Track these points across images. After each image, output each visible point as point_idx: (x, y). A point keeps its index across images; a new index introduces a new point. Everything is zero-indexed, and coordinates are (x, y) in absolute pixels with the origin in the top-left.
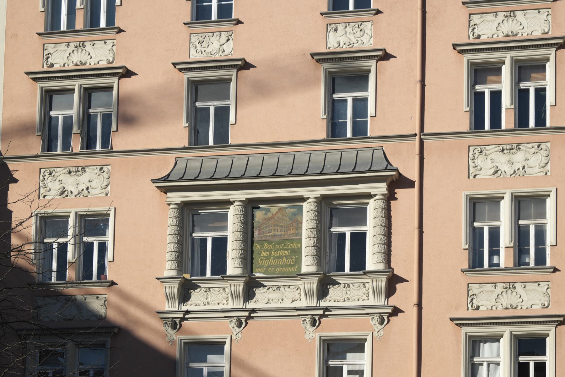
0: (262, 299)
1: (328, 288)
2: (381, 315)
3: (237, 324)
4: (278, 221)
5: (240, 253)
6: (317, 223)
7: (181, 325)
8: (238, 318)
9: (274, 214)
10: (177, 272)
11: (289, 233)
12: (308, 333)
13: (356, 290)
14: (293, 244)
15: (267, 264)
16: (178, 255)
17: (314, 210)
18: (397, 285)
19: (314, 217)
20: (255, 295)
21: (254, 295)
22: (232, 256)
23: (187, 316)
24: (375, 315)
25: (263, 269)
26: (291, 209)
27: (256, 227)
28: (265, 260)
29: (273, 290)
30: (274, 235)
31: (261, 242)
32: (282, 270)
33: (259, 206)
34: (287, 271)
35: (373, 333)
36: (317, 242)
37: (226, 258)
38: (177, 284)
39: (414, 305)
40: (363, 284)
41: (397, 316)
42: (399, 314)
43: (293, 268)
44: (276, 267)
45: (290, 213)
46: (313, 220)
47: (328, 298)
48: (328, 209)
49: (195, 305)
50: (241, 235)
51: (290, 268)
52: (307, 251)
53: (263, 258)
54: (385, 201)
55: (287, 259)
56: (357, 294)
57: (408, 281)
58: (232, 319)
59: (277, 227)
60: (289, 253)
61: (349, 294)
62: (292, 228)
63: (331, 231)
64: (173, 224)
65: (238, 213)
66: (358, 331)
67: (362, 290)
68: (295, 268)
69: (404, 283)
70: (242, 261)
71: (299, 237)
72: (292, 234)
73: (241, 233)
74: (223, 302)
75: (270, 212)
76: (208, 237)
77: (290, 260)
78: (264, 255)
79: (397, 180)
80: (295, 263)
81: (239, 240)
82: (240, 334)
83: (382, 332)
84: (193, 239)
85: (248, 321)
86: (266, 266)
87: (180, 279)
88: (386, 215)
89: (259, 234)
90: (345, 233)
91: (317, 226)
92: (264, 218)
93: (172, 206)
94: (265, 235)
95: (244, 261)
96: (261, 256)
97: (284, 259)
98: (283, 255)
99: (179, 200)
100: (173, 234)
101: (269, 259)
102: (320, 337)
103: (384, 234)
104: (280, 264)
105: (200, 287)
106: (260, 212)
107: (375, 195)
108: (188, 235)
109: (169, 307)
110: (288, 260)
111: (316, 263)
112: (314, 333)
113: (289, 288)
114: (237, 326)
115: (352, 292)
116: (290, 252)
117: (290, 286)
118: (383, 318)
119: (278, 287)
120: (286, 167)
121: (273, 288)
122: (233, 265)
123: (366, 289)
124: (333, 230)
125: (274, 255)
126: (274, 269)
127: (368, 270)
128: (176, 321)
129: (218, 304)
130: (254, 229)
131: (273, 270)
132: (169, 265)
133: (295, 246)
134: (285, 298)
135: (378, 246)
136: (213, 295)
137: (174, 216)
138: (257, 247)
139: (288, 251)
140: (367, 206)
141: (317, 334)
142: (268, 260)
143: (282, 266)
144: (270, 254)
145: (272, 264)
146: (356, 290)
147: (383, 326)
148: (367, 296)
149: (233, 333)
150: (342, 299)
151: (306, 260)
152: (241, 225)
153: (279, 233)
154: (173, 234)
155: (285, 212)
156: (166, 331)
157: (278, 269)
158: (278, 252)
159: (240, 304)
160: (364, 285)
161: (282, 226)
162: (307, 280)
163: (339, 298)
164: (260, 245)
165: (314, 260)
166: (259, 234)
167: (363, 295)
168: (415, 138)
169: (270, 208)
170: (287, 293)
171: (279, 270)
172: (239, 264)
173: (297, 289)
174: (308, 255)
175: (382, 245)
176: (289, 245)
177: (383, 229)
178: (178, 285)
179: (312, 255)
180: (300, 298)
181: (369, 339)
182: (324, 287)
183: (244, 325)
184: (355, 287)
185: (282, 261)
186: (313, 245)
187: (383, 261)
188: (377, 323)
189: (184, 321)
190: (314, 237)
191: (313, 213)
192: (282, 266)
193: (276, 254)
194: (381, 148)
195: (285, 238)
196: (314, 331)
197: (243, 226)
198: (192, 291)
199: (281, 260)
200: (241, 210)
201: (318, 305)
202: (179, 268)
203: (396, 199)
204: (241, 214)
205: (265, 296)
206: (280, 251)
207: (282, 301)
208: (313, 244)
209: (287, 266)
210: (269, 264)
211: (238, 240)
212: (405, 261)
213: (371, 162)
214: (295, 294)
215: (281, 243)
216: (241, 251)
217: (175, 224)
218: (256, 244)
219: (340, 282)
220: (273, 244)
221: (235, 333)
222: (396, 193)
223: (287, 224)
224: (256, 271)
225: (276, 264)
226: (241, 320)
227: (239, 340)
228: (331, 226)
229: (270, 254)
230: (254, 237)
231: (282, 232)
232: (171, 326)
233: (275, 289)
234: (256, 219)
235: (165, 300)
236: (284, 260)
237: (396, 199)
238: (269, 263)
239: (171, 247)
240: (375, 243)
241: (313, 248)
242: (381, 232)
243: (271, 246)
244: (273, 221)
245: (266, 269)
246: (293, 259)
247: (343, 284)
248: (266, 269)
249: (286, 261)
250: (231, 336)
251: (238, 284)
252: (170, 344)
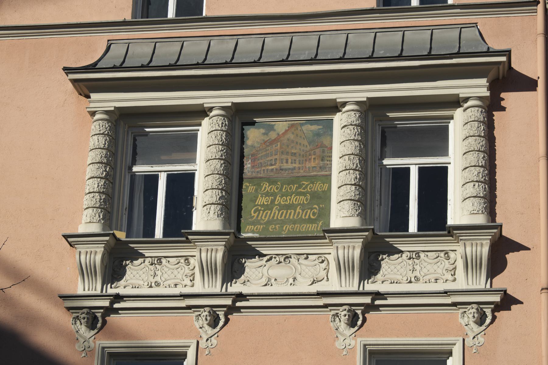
0: (257, 278)
1: (379, 259)
2: (481, 306)
3: (210, 320)
4: (288, 146)
5: (218, 195)
6: (360, 147)
7: (104, 323)
8: (212, 310)
9: (281, 133)
10: (101, 228)
11: (307, 166)
12: (341, 338)
13: (431, 264)
14: (315, 185)
15: (267, 219)
16: (104, 199)
17: (355, 123)
18: (507, 256)
19: (355, 136)
20: (244, 270)
21: (241, 271)
22: (205, 201)
23: (116, 306)
24: (469, 307)
25: (259, 226)
26: (311, 125)
27: (249, 155)
28: (264, 211)
29: (278, 262)
30: (281, 169)
31: (257, 181)
32: (294, 229)
33: (255, 119)
34: (304, 230)
35: (464, 340)
36: (360, 178)
37: (192, 207)
38: (101, 247)
39: (542, 289)
40: (444, 252)
41: (510, 309)
42: (513, 307)
43: (314, 225)
44: (283, 222)
45: (310, 132)
46: (354, 140)
47: (379, 276)
48: (378, 127)
49: (133, 288)
50: (221, 165)
51: (308, 225)
52: (341, 194)
53: (260, 208)
54: (484, 110)
55: (303, 211)
56: (433, 271)
57: (529, 249)
58: (200, 311)
59: (286, 156)
60: (307, 200)
61: (418, 271)
62: (313, 157)
63: (384, 164)
64: (98, 145)
65: (217, 128)
66: (435, 336)
67: (443, 263)
68: (318, 224)
69: (522, 252)
70: (221, 210)
71: (326, 173)
72: (314, 167)
73: (222, 162)
74: (184, 283)
75: (275, 130)
76: (159, 173)
77: (309, 211)
78: (262, 203)
79: (503, 77)
80: (319, 216)
81: (218, 174)
82: (215, 339)
83: (481, 339)
84: (133, 176)
85: (229, 316)
86: (265, 221)
87: (107, 238)
88: (486, 134)
89: (254, 166)
90: (409, 168)
91: (360, 150)
92: (263, 140)
93: (97, 116)
94: (264, 168)
95: (225, 209)
96: (257, 203)
97: (298, 210)
98: (297, 203)
99: (110, 106)
100: (99, 163)
101: (271, 209)
102: (365, 345)
103: (484, 165)
104: (291, 218)
105: (142, 256)
106: (256, 130)
107: (466, 99)
108: (125, 169)
109: (84, 290)
110: (305, 211)
111: (359, 213)
112: (353, 339)
113: (307, 258)
114: (209, 325)
115: (423, 267)
116: (309, 197)
117: (309, 256)
118: (483, 313)
119: (287, 257)
120: (305, 54)
121: (278, 259)
122: (205, 216)
123: (449, 262)
124: (386, 162)
125: (280, 202)
126: (279, 227)
127: (459, 223)
128: (97, 314)
129: (176, 285)
130: (245, 158)
131: (277, 228)
132: (88, 216)
133: (318, 187)
134: (298, 277)
135: (474, 185)
136: (166, 269)
137: (102, 132)
138: (248, 188)
139: (305, 197)
140: (449, 123)
141: (359, 340)
142: (269, 212)
143: (294, 222)
144: (273, 201)
145: (275, 218)
146: (431, 264)
147: (483, 327)
148: (453, 274)
149: (201, 337)
150: (405, 278)
151: (340, 208)
152: (223, 149)
153: (290, 166)
154: (99, 163)
155: (301, 130)
156: (77, 332)
157: (286, 227)
158: (275, 225)
159: (216, 286)
160: (446, 255)
161: (295, 154)
162: (341, 243)
163: (399, 277)
164: (255, 185)
165: (356, 208)
166: (253, 167)
167: (444, 272)
168: (535, 8)
169: (273, 123)
170: (304, 267)
171: (289, 229)
172: (216, 214)
173: (323, 262)
174: (344, 199)
175: (480, 184)
176: (307, 185)
177: (482, 156)
178: (103, 249)
179: (351, 200)
180: (327, 276)
181: (457, 351)
182: (372, 257)
183: (221, 323)
184: (430, 259)
185: (295, 213)
186: (353, 183)
187: (482, 211)
188: (472, 320)
189: (111, 316)
190: (355, 170)
191: (354, 129)
192: (294, 222)
193: (283, 202)
194: (474, 25)
195: (299, 174)
196: (354, 335)
197: (225, 151)
198: (128, 262)
199: (293, 211)
200: (222, 123)
201: (361, 288)
202: (105, 221)
203: (503, 109)
204: (222, 130)
205: (262, 274)
206: (291, 196)
207: (294, 281)
208: (353, 180)
209: (302, 221)
210: (271, 218)
211: (216, 172)
212: (522, 214)
213: (458, 45)
214: (318, 270)
215: (293, 183)
216: (222, 193)
217: (102, 146)
218: (248, 184)
219: (403, 250)
220: (278, 183)
221: (205, 337)
222: (503, 99)
223: (303, 151)
224: (247, 229)
225: (283, 218)
226: (218, 313)
227: (212, 350)
228: (382, 158)
229: (273, 201)
230: (244, 171)
231: (295, 163)
232: (87, 322)
233: (282, 260)
234: (249, 142)
235: (77, 278)
236: (297, 212)
237: (503, 109)
238: (270, 216)
239: (94, 185)
240: (468, 181)
241: (354, 187)
242: (478, 161)
243: (274, 187)
244: (279, 146)
245: (264, 226)
246: (316, 211)
247: (408, 253)
248: (264, 226)
249: (302, 214)
250: (198, 342)
251: (214, 248)
252: (83, 355)
